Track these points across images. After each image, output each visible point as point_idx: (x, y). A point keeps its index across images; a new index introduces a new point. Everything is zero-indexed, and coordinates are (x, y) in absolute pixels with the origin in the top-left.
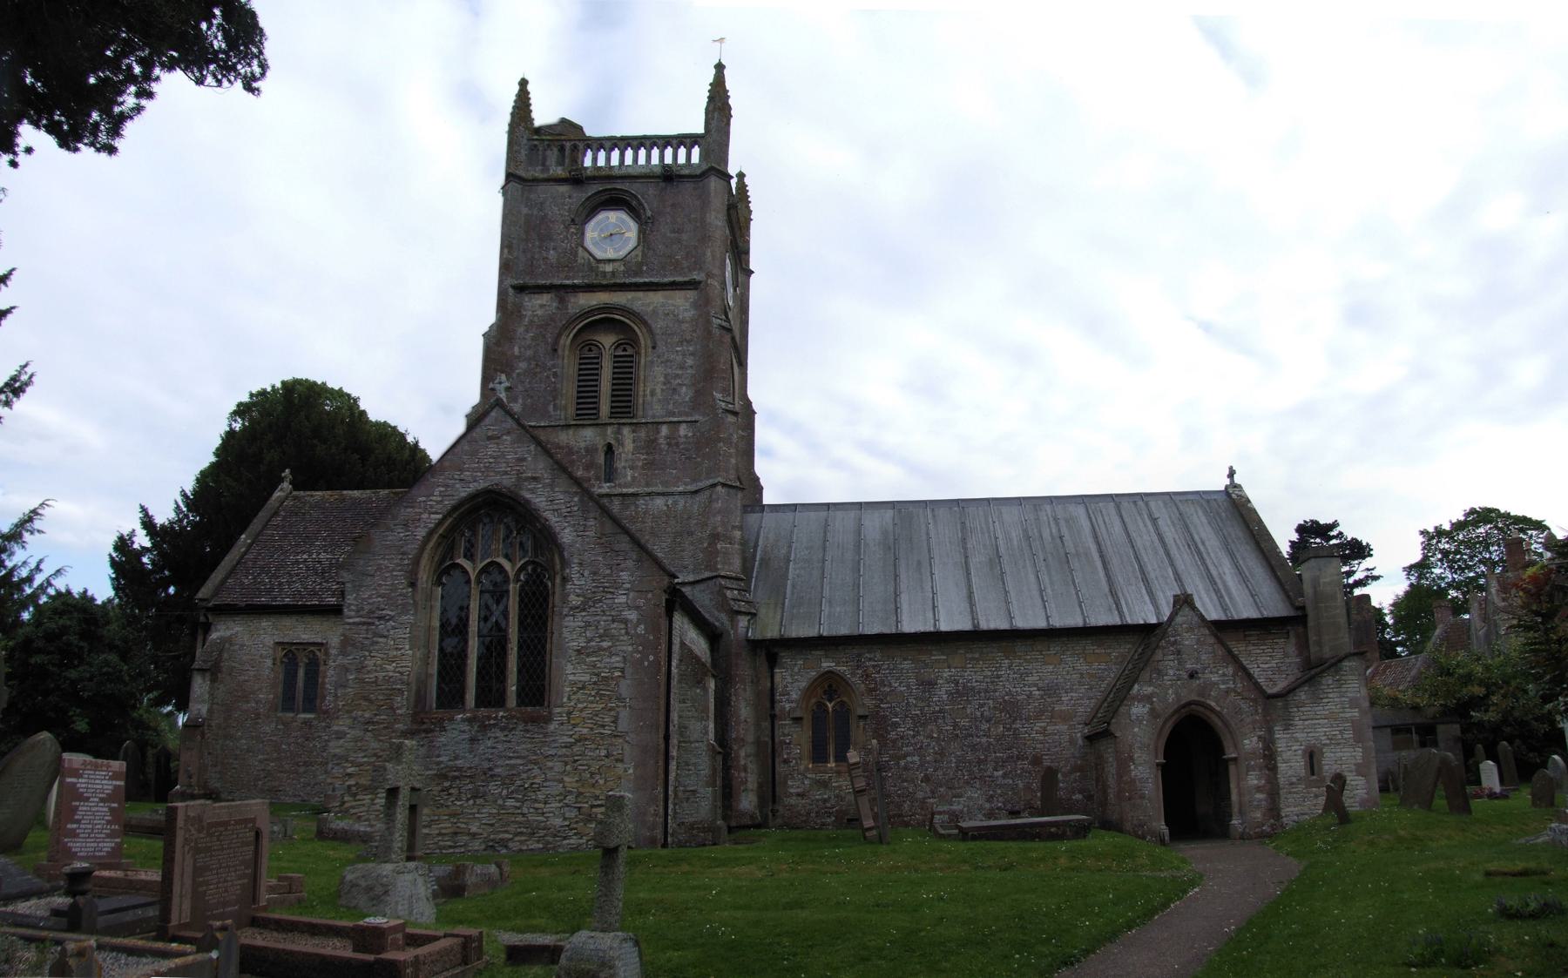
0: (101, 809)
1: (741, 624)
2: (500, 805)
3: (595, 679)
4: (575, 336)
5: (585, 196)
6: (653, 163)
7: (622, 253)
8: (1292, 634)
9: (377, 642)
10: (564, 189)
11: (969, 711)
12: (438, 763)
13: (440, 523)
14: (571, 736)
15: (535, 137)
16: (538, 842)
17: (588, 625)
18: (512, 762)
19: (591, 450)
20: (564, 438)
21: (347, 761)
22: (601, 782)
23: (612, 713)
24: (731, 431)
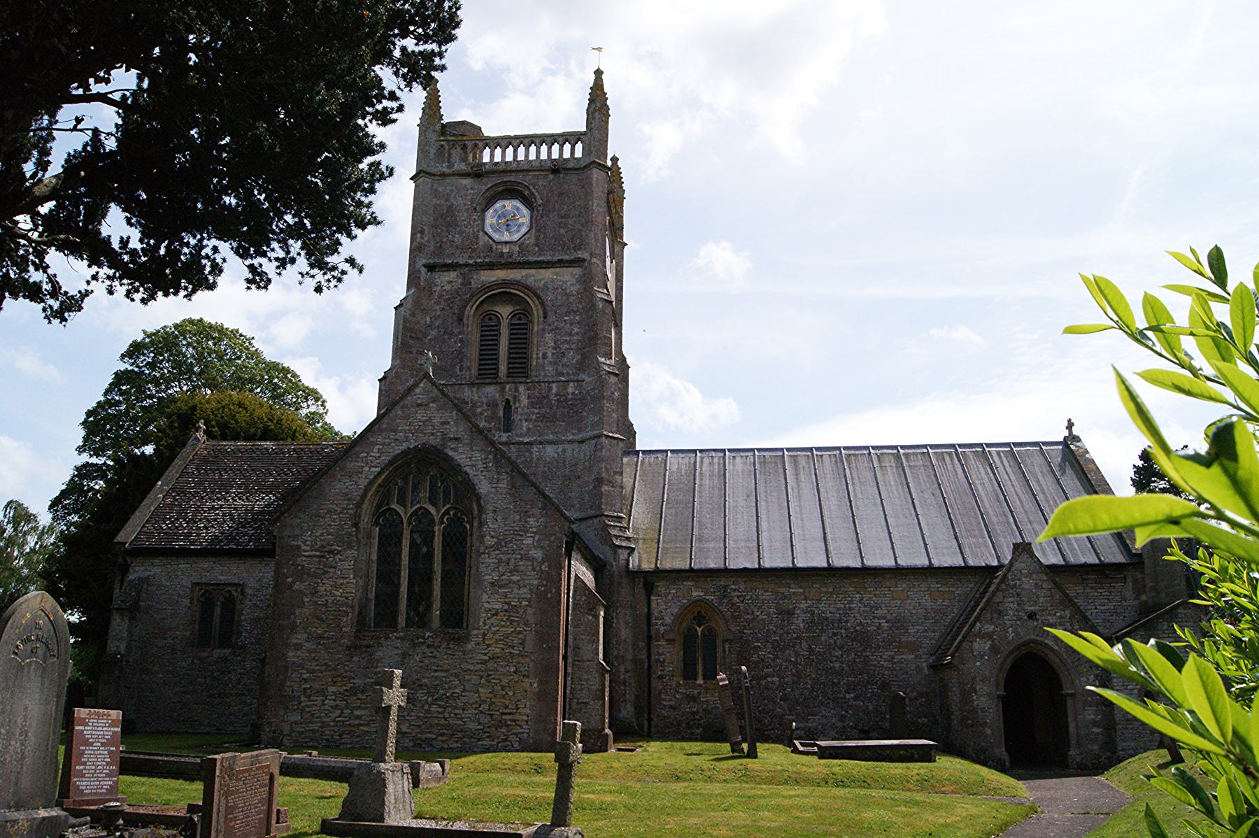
0: (102, 752)
1: (622, 557)
2: (426, 710)
3: (506, 607)
4: (477, 308)
5: (484, 188)
6: (531, 158)
7: (516, 237)
8: (1129, 580)
9: (327, 572)
10: (466, 182)
11: (823, 639)
12: (376, 673)
13: (380, 474)
14: (485, 654)
15: (442, 138)
16: (457, 742)
17: (500, 561)
18: (436, 674)
19: (492, 405)
20: (467, 393)
21: (303, 668)
22: (511, 694)
23: (520, 636)
24: (613, 389)
